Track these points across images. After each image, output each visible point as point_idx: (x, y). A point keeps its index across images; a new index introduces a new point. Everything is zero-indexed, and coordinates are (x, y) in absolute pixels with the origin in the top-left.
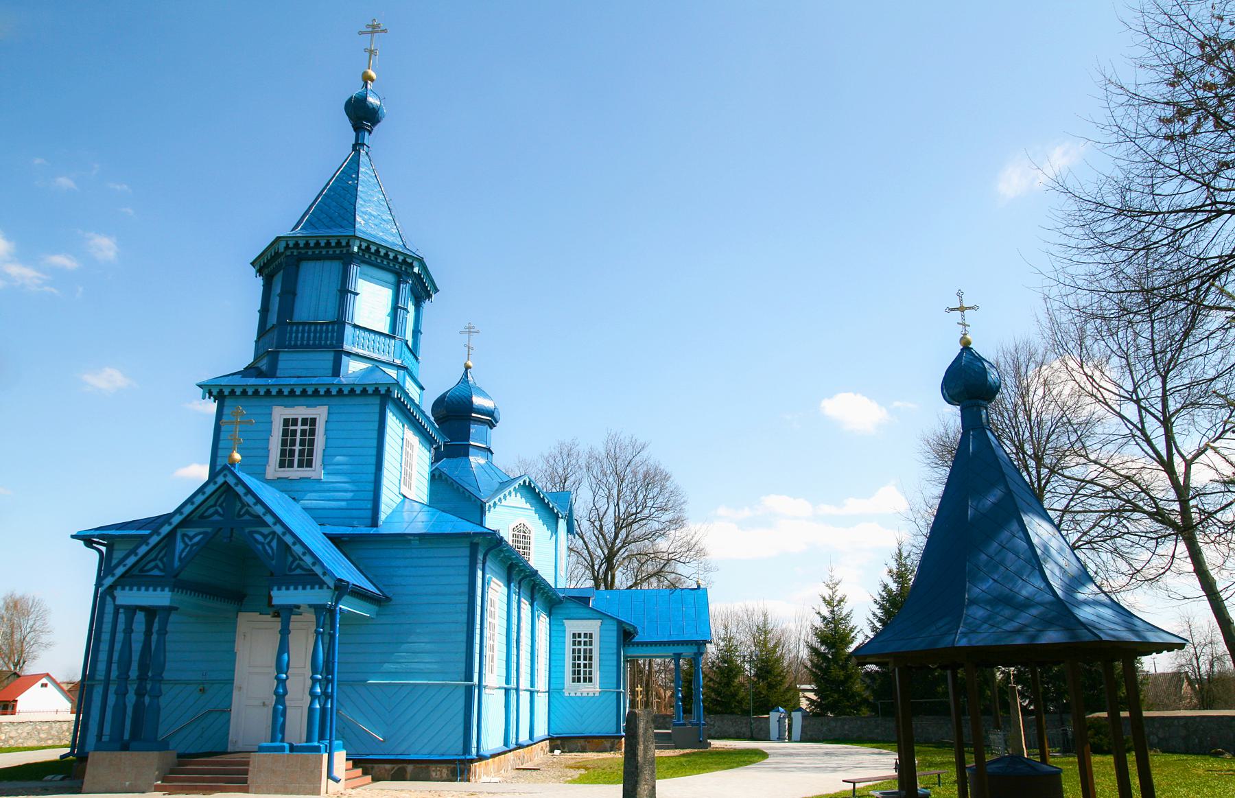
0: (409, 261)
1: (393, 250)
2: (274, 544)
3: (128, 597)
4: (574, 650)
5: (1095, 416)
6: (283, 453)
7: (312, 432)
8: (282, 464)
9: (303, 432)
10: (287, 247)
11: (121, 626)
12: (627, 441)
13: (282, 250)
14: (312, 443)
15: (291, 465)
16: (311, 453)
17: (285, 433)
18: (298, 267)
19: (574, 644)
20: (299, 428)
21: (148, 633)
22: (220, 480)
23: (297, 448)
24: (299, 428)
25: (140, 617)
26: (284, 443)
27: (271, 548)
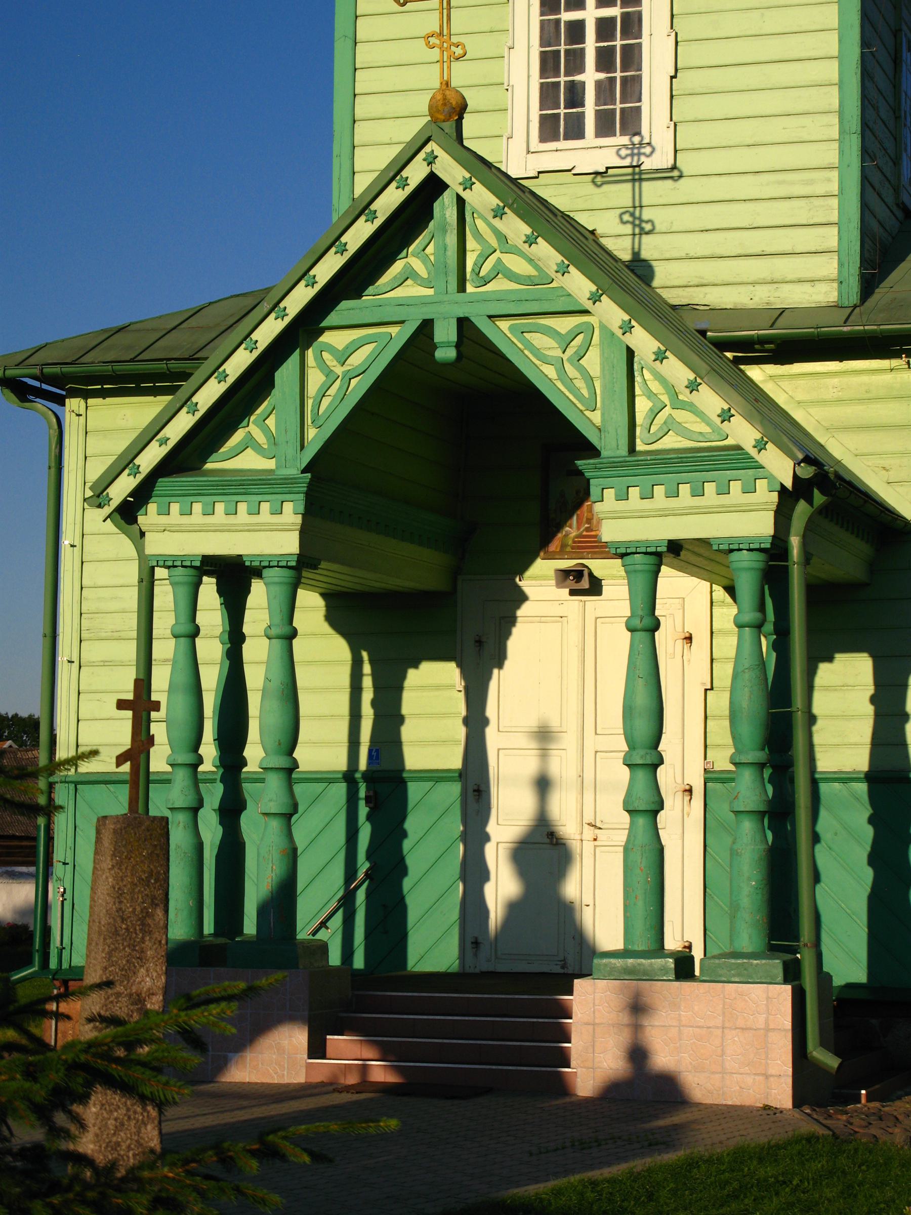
2: (593, 361)
6: (548, 94)
8: (549, 129)
11: (165, 620)
14: (632, 57)
15: (576, 131)
22: (416, 173)
23: (590, 76)
25: (209, 588)
26: (548, 63)
27: (584, 372)
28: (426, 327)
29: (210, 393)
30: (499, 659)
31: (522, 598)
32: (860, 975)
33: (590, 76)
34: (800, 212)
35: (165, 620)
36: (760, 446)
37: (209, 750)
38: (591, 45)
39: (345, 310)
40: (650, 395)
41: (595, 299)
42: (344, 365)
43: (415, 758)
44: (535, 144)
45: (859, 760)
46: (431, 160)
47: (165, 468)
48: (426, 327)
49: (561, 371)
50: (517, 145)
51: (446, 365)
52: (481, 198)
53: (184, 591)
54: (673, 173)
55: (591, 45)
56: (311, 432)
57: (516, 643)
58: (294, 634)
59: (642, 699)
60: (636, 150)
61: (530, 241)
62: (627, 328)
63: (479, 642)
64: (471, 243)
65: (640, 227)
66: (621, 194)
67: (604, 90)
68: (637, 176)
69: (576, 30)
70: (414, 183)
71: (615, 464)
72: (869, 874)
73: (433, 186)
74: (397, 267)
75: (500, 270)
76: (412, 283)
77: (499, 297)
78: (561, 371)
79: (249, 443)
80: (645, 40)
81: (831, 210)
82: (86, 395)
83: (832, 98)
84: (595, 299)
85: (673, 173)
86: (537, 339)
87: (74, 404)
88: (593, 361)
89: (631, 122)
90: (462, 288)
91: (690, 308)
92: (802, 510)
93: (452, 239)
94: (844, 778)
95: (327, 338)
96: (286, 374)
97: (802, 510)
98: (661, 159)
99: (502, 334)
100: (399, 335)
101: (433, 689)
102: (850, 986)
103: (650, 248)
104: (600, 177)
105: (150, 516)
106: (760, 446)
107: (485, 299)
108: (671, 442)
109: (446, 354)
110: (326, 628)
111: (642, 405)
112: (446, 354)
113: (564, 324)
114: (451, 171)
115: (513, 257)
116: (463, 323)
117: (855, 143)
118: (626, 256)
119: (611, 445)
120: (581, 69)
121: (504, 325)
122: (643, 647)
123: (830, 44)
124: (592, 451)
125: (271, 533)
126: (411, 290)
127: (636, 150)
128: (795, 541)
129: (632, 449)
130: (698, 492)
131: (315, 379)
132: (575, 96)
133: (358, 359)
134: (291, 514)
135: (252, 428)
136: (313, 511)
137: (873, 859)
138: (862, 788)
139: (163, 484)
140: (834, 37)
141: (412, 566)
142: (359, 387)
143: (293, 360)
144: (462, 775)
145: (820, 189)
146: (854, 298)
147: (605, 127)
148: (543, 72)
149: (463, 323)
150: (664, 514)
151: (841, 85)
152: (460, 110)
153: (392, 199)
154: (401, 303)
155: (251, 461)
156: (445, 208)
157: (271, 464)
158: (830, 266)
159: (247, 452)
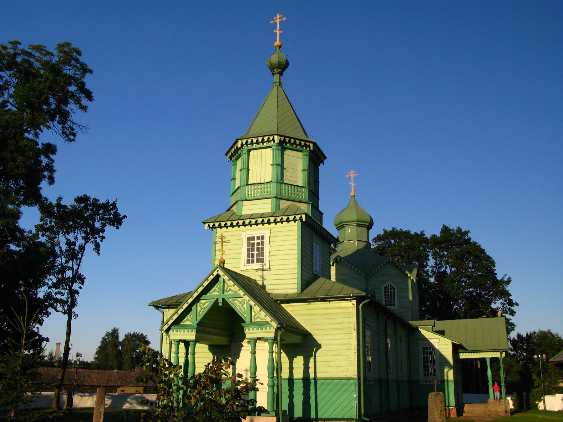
0: (308, 144)
1: (288, 137)
2: (245, 306)
3: (479, 362)
4: (424, 358)
5: (39, 131)
6: (248, 255)
7: (263, 243)
8: (248, 262)
9: (258, 244)
10: (242, 145)
11: (173, 350)
12: (54, 202)
13: (240, 146)
14: (263, 249)
15: (253, 262)
16: (262, 254)
17: (249, 245)
18: (249, 155)
19: (424, 353)
20: (256, 241)
21: (187, 354)
22: (215, 273)
23: (255, 252)
24: (256, 241)
25: (182, 345)
26: (248, 250)
27: (244, 308)
28: (217, 299)
29: (180, 311)
30: (238, 357)
31: (242, 346)
32: (301, 415)
33: (255, 252)
34: (291, 276)
35: (173, 350)
36: (271, 321)
37: (275, 375)
38: (256, 247)
39: (204, 297)
40: (255, 312)
41: (244, 295)
42: (204, 305)
43: (295, 376)
44: (246, 264)
45: (301, 376)
46: (218, 271)
47: (173, 324)
48: (217, 299)
49: (240, 308)
50: (243, 264)
51: (220, 307)
52: (226, 278)
53: (176, 346)
54: (269, 269)
55: (256, 247)
56: (198, 318)
57: (241, 354)
58: (195, 353)
59: (253, 365)
60: (263, 265)
61: (234, 285)
62: (249, 301)
63: (235, 354)
64: (225, 285)
65: (264, 279)
66: (261, 273)
67: (258, 255)
68: (263, 270)
69: (253, 244)
70: (215, 275)
71: (248, 324)
72: (303, 396)
73: (218, 276)
74: (213, 289)
75: (230, 290)
76: (215, 292)
77: (230, 295)
78: (240, 308)
79: (188, 319)
80: (265, 246)
81: (296, 276)
82: (168, 308)
83: (296, 256)
84: (244, 295)
85: (269, 269)
86: (236, 302)
87: (166, 310)
88: (245, 306)
89: (262, 261)
90: (223, 293)
91: (271, 293)
92: (280, 333)
93: (222, 284)
94: (298, 379)
95: (201, 301)
96: (194, 308)
97: (280, 333)
98: (267, 267)
99: (230, 301)
100: (213, 301)
101: (299, 361)
102: (299, 417)
103: (265, 283)
104: (257, 270)
105: (171, 332)
106: (271, 321)
107: (227, 295)
108: (258, 320)
109: (220, 304)
110: (208, 351)
111: (253, 314)
112: (220, 304)
113: (240, 299)
114: (221, 273)
115: (232, 288)
116: (223, 299)
117: (300, 264)
118: (261, 284)
119: (248, 320)
120: (254, 251)
121: (230, 299)
122: (253, 357)
123: (296, 247)
124: (244, 322)
125: (191, 336)
126: (215, 293)
127: (263, 265)
128: (279, 338)
129: (251, 321)
130: (262, 329)
131: (199, 308)
132: (253, 256)
133: (206, 305)
134: (194, 332)
135: (188, 317)
136: (197, 332)
137: (303, 394)
138: (302, 381)
139: (173, 327)
140: (297, 246)
141: (220, 340)
142: (206, 310)
143: (195, 305)
144: (288, 379)
145: (294, 272)
146: (300, 292)
147: (258, 261)
148: (248, 252)
149: (223, 299)
150: (256, 333)
151: (298, 254)
152: (224, 263)
153: (211, 278)
154: (213, 296)
155: (188, 323)
156: (221, 280)
157: (191, 323)
158: (296, 286)
159: (187, 321)
